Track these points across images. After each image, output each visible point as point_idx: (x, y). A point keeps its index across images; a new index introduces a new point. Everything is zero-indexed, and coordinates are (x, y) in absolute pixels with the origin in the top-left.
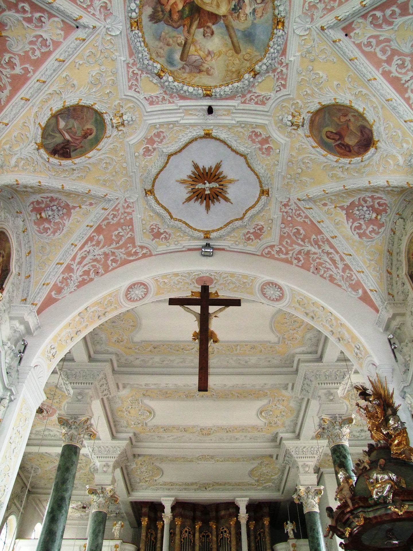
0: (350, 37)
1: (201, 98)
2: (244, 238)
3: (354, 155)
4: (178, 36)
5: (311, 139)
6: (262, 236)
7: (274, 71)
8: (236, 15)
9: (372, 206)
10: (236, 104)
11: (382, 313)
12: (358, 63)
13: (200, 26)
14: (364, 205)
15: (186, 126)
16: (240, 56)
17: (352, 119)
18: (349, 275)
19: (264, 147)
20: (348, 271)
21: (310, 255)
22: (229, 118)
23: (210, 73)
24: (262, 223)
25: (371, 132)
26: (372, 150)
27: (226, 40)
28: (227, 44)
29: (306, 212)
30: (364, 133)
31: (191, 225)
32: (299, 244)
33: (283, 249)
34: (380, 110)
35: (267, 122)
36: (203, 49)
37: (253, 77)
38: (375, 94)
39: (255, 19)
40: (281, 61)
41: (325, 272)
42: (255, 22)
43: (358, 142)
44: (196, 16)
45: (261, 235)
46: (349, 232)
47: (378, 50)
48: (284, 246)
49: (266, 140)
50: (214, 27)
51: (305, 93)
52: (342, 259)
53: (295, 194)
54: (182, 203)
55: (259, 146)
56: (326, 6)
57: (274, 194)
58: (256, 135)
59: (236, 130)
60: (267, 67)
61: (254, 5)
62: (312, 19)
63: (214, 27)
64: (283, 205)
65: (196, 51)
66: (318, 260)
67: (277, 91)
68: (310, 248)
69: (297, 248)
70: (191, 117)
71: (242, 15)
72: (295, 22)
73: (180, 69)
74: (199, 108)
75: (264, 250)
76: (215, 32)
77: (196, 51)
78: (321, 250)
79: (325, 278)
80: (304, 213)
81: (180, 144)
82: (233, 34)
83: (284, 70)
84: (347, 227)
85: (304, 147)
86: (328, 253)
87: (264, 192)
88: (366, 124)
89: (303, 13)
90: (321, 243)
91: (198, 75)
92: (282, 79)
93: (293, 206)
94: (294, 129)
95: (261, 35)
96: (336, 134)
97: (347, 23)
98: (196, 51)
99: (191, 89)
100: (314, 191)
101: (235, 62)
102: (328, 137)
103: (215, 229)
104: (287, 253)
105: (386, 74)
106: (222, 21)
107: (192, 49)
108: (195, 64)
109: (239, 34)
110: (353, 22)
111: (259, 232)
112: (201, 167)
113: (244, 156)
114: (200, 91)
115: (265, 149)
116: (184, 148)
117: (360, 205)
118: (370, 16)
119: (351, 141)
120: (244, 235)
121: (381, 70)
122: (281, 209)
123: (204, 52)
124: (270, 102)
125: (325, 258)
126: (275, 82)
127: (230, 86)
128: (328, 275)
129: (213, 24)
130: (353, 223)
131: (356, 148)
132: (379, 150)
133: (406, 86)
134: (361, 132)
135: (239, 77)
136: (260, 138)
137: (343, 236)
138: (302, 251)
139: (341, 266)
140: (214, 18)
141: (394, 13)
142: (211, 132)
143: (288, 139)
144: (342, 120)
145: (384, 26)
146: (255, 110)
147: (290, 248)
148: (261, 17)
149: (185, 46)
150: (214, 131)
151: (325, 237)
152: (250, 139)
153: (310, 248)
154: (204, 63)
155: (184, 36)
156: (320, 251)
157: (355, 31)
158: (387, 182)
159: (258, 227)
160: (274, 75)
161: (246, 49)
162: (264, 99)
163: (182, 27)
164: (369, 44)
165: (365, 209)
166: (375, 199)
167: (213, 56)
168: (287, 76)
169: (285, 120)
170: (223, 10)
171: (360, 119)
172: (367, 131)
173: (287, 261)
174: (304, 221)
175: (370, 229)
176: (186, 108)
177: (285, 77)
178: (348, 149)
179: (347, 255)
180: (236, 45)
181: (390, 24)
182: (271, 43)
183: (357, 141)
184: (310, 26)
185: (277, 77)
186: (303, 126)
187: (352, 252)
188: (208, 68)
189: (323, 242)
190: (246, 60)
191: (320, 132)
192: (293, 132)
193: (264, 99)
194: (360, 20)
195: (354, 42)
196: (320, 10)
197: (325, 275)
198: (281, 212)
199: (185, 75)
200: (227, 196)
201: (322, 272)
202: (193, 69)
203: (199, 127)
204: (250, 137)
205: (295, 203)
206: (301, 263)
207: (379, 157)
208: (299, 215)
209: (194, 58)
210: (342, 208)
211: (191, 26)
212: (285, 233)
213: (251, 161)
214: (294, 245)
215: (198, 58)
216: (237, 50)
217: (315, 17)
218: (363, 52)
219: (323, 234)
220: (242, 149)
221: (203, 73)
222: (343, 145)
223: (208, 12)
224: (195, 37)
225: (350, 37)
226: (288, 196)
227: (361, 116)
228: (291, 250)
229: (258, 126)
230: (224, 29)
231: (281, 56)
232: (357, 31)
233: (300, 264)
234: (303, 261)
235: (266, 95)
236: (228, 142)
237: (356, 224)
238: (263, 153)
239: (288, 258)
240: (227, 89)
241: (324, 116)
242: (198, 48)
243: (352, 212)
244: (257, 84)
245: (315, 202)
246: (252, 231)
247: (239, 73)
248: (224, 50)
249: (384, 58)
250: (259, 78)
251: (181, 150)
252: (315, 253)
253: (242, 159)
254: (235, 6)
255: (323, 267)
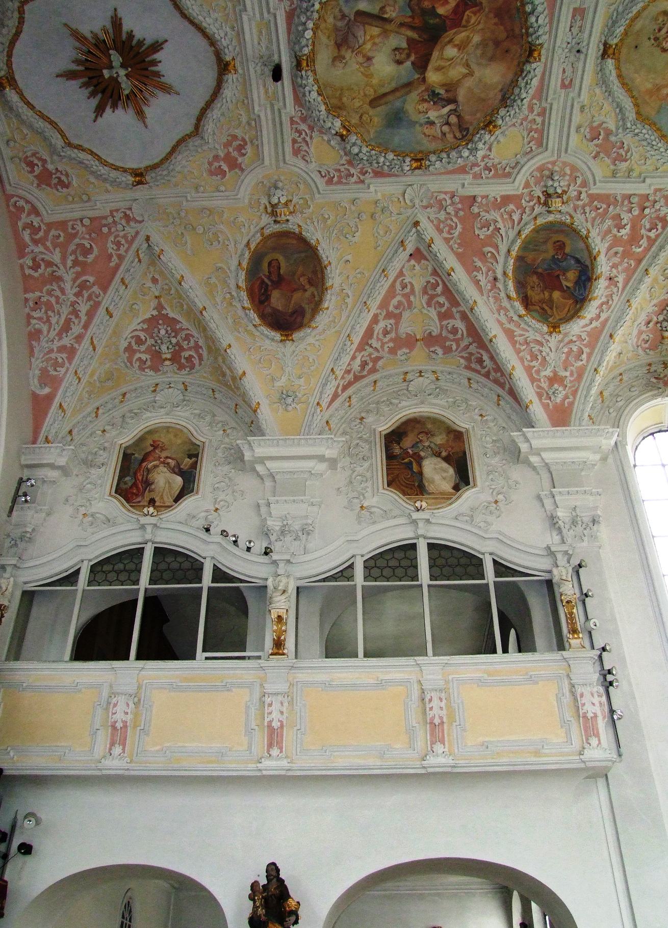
0: (409, 261)
1: (292, 49)
2: (29, 154)
3: (258, 310)
4: (397, 7)
5: (258, 237)
6: (49, 188)
7: (350, 163)
8: (426, 97)
9: (182, 349)
10: (288, 110)
11: (52, 450)
12: (382, 283)
13: (410, 41)
14: (179, 337)
15: (240, 34)
16: (367, 107)
17: (308, 294)
18: (60, 360)
19: (222, 163)
20: (64, 355)
21: (54, 284)
22: (263, 102)
23: (337, 63)
24: (74, 183)
25: (300, 326)
26: (277, 336)
27: (389, 83)
28: (383, 86)
29: (130, 252)
30: (295, 316)
31: (18, 45)
32: (64, 258)
33: (41, 234)
34: (334, 330)
35: (267, 162)
36: (374, 48)
37: (337, 133)
38: (351, 318)
39: (421, 125)
40: (366, 172)
41: (40, 319)
42: (417, 126)
43: (279, 311)
44: (425, 37)
45: (49, 185)
46: (127, 333)
47: (399, 298)
48: (47, 232)
49: (234, 164)
50: (408, 64)
51: (327, 217)
52: (79, 338)
53: (153, 229)
54: (64, 21)
55: (222, 154)
56: (443, 222)
57: (141, 192)
58: (240, 148)
59: (242, 112)
60: (357, 154)
61: (439, 122)
62: (426, 207)
63: (408, 64)
64: (125, 213)
65: (372, 37)
66: (53, 300)
67: (320, 172)
68: (68, 277)
69: (56, 257)
70: (255, 31)
71: (426, 105)
72: (421, 185)
73: (341, 11)
74: (275, 47)
75: (21, 198)
76: (401, 67)
77: (372, 37)
78: (75, 299)
79: (29, 323)
80: (126, 251)
81: (200, 18)
82: (398, 94)
83: (355, 179)
84: (134, 325)
85: (243, 230)
86: (75, 313)
87: (139, 177)
88: (308, 316)
89: (433, 192)
90: (86, 294)
91: (333, 42)
92: (340, 177)
93: (130, 231)
94: (266, 208)
95: (401, 136)
96: (279, 274)
97: (425, 253)
98: (371, 36)
99: (309, 34)
100: (174, 260)
101: (356, 101)
102: (270, 264)
103: (25, 94)
104: (36, 242)
105: (375, 320)
106: (417, 76)
107: (375, 31)
108: (351, 38)
109: (398, 104)
110: (427, 260)
111: (55, 181)
112: (157, 56)
113: (197, 129)
114: (306, 51)
115: (220, 166)
116: (192, 23)
117: (176, 332)
118: (436, 280)
119: (277, 300)
120: (34, 155)
121: (379, 311)
122: (117, 211)
123: (370, 50)
124: (302, 164)
125: (65, 311)
126: (333, 167)
127: (320, 99)
128: (37, 326)
129: (413, 63)
130: (143, 330)
131: (268, 310)
132: (280, 345)
133: (367, 347)
134: (294, 312)
135: (336, 109)
136: (235, 154)
137: (117, 325)
138: (55, 268)
139: (66, 341)
140: (422, 65)
141: (442, 305)
142: (233, 72)
143: (246, 201)
144: (302, 279)
145: (426, 297)
146: (283, 142)
147: (49, 244)
148: (424, 134)
149: (379, 19)
150: (235, 76)
151: (100, 299)
152: (230, 138)
153: (68, 277)
154: (353, 51)
155: (396, 17)
156: (73, 298)
157: (416, 265)
158: (244, 373)
159: (64, 178)
160: (343, 165)
161: (377, 116)
162: (303, 153)
163: (410, 14)
164: (404, 287)
165: (174, 341)
166: (197, 352)
167: (365, 65)
168: (346, 183)
169: (279, 193)
170: (433, 77)
171: (312, 306)
172: (299, 320)
173: (21, 250)
174: (111, 256)
175: (144, 357)
176: (272, 25)
177: (344, 181)
178: (263, 298)
179: (92, 343)
180: (383, 101)
181: (429, 304)
182: (391, 156)
183: (280, 308)
184: (417, 206)
185: (342, 169)
186: (275, 222)
187: (99, 350)
188: (344, 58)
189: (90, 298)
190: (361, 117)
191: (274, 249)
192: (262, 208)
193: (303, 153)
194: (430, 269)
195: (403, 267)
196: (438, 216)
197: (33, 321)
198: (111, 212)
199: (330, 20)
200: (108, 110)
201: (36, 314)
202: (341, 33)
203: (237, 49)
204: (235, 137)
205: (137, 233)
206: (32, 272)
207: (271, 348)
208: (118, 244)
209: (360, 33)
210: (160, 307)
211: (412, 28)
212: (73, 228)
213: (191, 143)
214: (58, 250)
215: (361, 42)
216: (374, 102)
217: (429, 210)
218: (395, 281)
219: (105, 293)
220: (209, 127)
221: (337, 51)
222: (266, 290)
223: (431, 54)
224: (393, 35)
225: (409, 261)
226: (146, 219)
227: (316, 305)
228: (47, 248)
229: (258, 151)
230: (405, 80)
231: (374, 171)
232: (417, 267)
233: (28, 272)
234: (36, 275)
235: (311, 155)
236: (217, 104)
237: (142, 335)
238: (210, 164)
239: (27, 246)
240: (314, 95)
241: (300, 252)
242: (377, 40)
243: (160, 325)
244: (326, 138)
245: (152, 263)
246: (50, 167)
247: (340, 108)
248: (375, 81)
249: (391, 308)
250: (335, 142)
251: (184, 16)
252: (63, 291)
253: (190, 129)
254: (438, 94)
255: (46, 313)
